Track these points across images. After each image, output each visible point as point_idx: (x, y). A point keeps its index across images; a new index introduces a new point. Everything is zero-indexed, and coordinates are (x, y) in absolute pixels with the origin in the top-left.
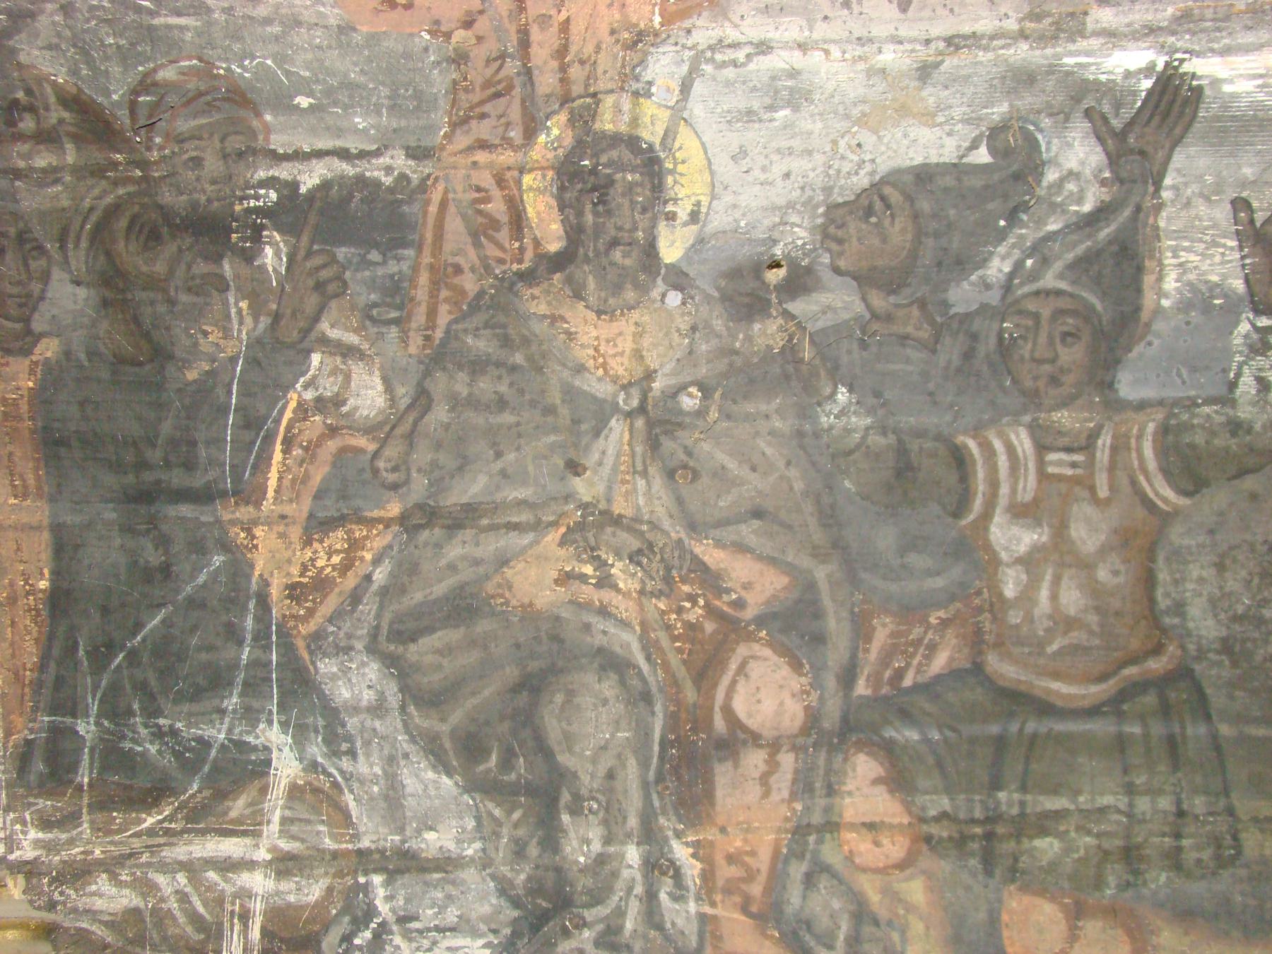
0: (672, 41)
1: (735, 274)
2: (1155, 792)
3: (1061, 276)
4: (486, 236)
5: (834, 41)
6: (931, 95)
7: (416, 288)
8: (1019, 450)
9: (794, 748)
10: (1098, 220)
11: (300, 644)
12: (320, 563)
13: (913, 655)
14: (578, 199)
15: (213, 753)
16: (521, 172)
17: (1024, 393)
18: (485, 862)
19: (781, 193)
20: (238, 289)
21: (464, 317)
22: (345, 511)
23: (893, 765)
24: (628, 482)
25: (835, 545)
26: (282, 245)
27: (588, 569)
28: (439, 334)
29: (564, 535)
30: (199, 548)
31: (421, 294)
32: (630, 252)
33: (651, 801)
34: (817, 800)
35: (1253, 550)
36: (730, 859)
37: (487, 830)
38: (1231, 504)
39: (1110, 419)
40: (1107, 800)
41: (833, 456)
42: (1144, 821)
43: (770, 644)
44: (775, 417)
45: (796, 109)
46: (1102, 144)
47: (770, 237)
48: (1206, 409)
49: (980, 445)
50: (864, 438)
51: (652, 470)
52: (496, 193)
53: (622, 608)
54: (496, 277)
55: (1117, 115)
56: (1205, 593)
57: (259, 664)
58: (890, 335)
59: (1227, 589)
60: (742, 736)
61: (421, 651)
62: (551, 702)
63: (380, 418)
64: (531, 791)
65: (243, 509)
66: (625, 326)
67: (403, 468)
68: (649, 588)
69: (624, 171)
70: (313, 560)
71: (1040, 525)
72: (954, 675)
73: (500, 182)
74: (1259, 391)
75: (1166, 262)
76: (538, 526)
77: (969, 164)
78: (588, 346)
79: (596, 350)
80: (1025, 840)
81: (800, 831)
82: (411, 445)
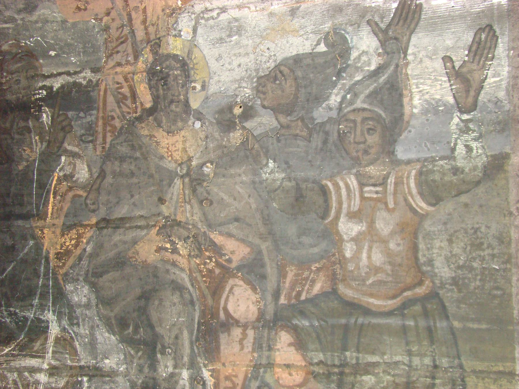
0: (186, 11)
1: (221, 112)
2: (422, 355)
3: (364, 102)
4: (123, 103)
5: (252, 3)
6: (296, 23)
7: (97, 127)
8: (351, 186)
9: (254, 328)
10: (379, 73)
11: (60, 277)
12: (67, 244)
13: (304, 285)
14: (156, 84)
15: (29, 323)
16: (134, 74)
17: (352, 158)
18: (126, 375)
19: (238, 73)
20: (35, 132)
21: (116, 138)
22: (76, 222)
23: (297, 337)
24: (183, 206)
25: (270, 233)
26: (49, 112)
27: (168, 246)
28: (108, 146)
29: (158, 230)
30: (24, 238)
31: (100, 129)
32: (178, 105)
33: (194, 349)
34: (264, 352)
35: (466, 232)
36: (227, 378)
37: (128, 360)
38: (455, 209)
39: (393, 169)
40: (398, 358)
41: (268, 192)
42: (416, 370)
43: (242, 279)
44: (243, 175)
45: (240, 35)
46: (377, 37)
47: (235, 94)
48: (441, 162)
49: (333, 184)
50: (281, 183)
51: (193, 201)
52: (125, 84)
53: (181, 262)
54: (127, 120)
55: (382, 22)
56: (443, 254)
57: (45, 285)
58: (290, 135)
59: (454, 253)
60: (231, 321)
61: (104, 280)
62: (153, 304)
63: (87, 182)
64: (145, 344)
65: (40, 222)
66: (178, 138)
67: (96, 203)
68: (192, 254)
69: (173, 70)
70: (65, 242)
71: (362, 222)
72: (324, 294)
73: (126, 79)
74: (467, 152)
75: (413, 91)
76: (148, 227)
77: (317, 52)
78: (165, 148)
79: (168, 149)
80: (358, 376)
81: (257, 367)
82: (99, 193)
